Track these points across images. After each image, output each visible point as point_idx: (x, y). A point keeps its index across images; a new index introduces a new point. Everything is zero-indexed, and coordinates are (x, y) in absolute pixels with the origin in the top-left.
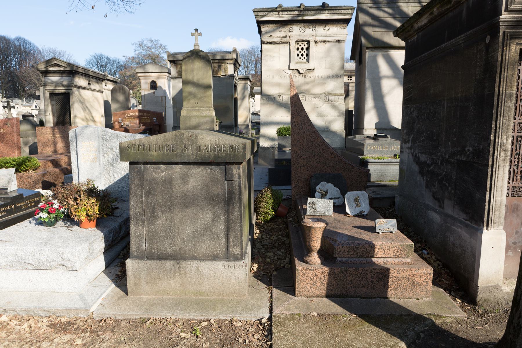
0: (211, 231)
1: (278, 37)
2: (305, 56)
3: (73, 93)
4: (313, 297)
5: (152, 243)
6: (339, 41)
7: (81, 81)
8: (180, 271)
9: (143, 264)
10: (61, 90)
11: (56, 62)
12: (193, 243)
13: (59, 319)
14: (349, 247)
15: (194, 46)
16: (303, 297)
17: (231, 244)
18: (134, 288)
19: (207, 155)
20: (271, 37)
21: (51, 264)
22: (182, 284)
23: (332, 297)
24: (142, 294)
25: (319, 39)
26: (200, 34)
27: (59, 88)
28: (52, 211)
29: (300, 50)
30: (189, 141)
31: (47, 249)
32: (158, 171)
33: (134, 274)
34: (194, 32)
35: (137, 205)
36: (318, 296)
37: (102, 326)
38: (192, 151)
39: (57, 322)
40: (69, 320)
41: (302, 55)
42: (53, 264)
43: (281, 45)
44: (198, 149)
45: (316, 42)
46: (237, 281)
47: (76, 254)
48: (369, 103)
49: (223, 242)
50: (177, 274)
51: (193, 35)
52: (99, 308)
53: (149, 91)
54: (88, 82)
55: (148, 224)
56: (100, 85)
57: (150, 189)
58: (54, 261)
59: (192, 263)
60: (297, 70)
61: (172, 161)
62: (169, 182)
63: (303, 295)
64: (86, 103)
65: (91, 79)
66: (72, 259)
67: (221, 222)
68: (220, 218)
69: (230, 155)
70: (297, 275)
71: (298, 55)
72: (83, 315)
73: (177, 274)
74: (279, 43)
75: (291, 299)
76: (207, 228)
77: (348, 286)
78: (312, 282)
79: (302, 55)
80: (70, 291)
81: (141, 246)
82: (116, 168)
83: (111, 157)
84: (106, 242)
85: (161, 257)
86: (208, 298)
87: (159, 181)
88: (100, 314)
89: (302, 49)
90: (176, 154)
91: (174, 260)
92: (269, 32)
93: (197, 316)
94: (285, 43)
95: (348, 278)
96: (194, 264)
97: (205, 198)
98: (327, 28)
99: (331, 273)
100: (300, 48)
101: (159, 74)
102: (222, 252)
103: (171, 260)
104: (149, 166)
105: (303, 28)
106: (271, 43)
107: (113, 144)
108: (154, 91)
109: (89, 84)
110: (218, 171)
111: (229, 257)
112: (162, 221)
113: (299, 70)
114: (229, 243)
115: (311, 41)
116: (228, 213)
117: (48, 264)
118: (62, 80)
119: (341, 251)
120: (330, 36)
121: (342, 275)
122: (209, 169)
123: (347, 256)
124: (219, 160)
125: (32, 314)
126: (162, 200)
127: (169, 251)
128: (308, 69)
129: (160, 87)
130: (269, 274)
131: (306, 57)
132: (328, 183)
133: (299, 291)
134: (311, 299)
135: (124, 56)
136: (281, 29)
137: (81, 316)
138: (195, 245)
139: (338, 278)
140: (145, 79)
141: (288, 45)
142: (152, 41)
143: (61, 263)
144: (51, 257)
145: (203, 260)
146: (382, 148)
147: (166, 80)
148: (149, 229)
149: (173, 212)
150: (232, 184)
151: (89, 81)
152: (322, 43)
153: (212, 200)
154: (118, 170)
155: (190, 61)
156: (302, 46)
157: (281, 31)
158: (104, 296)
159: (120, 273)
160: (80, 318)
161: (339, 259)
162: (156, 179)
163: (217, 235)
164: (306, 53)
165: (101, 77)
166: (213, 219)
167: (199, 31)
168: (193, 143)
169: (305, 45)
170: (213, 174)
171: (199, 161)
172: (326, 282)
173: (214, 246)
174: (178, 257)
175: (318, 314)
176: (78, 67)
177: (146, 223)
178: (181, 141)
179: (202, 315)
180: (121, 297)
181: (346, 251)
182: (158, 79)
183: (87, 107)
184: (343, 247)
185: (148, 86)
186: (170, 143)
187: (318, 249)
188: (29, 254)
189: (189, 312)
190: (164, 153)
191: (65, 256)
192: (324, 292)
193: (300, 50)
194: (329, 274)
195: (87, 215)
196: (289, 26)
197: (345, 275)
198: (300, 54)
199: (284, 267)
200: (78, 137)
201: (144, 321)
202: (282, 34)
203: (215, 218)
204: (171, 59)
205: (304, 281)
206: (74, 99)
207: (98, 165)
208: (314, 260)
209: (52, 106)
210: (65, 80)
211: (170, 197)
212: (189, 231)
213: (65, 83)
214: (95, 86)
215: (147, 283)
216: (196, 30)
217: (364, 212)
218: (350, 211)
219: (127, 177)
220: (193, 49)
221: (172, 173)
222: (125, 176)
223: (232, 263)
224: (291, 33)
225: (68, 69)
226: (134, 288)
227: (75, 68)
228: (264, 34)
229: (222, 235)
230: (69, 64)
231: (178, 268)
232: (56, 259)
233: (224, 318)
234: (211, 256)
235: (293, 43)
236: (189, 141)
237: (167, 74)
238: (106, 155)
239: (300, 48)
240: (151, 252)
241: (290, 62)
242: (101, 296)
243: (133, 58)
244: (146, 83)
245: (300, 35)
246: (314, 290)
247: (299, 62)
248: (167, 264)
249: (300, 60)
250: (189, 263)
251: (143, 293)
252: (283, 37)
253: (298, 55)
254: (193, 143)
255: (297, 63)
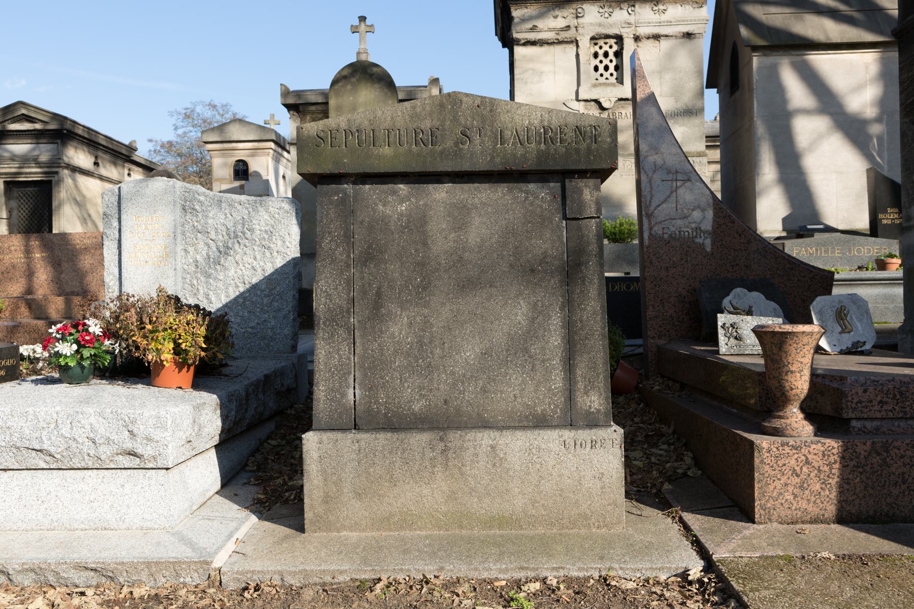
0: (526, 350)
1: (550, 30)
2: (612, 69)
3: (60, 181)
4: (803, 522)
5: (371, 388)
6: (688, 36)
7: (80, 157)
8: (447, 460)
9: (348, 443)
10: (33, 173)
11: (24, 111)
12: (481, 383)
13: (125, 590)
14: (881, 391)
15: (358, 53)
16: (775, 524)
17: (581, 385)
18: (320, 509)
19: (520, 151)
20: (534, 29)
21: (102, 449)
22: (452, 496)
23: (856, 522)
24: (344, 528)
25: (643, 31)
26: (371, 29)
27: (28, 170)
28: (87, 342)
29: (601, 57)
30: (474, 119)
31: (91, 410)
32: (390, 198)
33: (323, 472)
34: (356, 22)
35: (336, 289)
36: (815, 521)
37: (252, 600)
38: (482, 142)
39: (122, 596)
40: (153, 592)
41: (606, 68)
42: (105, 451)
43: (558, 49)
44: (496, 138)
45: (637, 39)
46: (599, 485)
47: (169, 422)
48: (768, 172)
49: (558, 381)
50: (438, 468)
51: (354, 30)
52: (233, 559)
53: (231, 183)
54: (93, 160)
55: (363, 336)
56: (120, 169)
57: (370, 247)
58: (108, 441)
59: (480, 435)
60: (597, 102)
61: (516, 71)
62: (417, 224)
63: (774, 517)
64: (89, 206)
65: (100, 154)
66: (157, 435)
67: (552, 328)
68: (550, 317)
69: (577, 151)
70: (757, 461)
71: (596, 69)
72: (193, 578)
73: (438, 468)
74: (553, 43)
75: (748, 528)
76: (521, 347)
77: (896, 491)
78: (798, 480)
79: (606, 68)
80: (149, 524)
81: (344, 395)
82: (216, 279)
83: (204, 253)
84: (224, 418)
85: (395, 423)
86: (522, 532)
87: (392, 223)
88: (242, 573)
89: (606, 55)
90: (442, 153)
91: (431, 428)
92: (531, 18)
93: (507, 570)
94: (567, 42)
95: (893, 469)
96: (485, 439)
97: (512, 266)
98: (661, 7)
99: (847, 455)
100: (601, 52)
101: (256, 144)
102: (556, 406)
103: (423, 430)
104: (367, 186)
105: (606, 9)
106: (533, 43)
107: (210, 221)
108: (243, 182)
109: (96, 164)
110: (542, 195)
111: (572, 418)
112: (399, 328)
113: (602, 100)
114: (576, 383)
115: (625, 36)
116: (570, 305)
117: (92, 453)
118: (36, 153)
119: (860, 402)
120: (669, 23)
121: (876, 460)
122: (521, 191)
123: (878, 415)
124: (552, 166)
125: (52, 579)
126: (401, 274)
127: (417, 407)
128: (621, 99)
129: (257, 174)
130: (654, 491)
131: (615, 73)
132: (750, 290)
133: (763, 508)
134: (798, 526)
135: (150, 141)
136: (557, 12)
137: (188, 580)
138: (484, 390)
139: (868, 469)
140: (223, 156)
141: (571, 49)
142: (215, 106)
143: (129, 445)
144: (102, 430)
145: (508, 428)
146: (826, 251)
147: (270, 160)
148: (365, 349)
149: (426, 305)
150: (579, 228)
151: (96, 157)
152: (651, 41)
153: (530, 272)
154: (220, 285)
155: (349, 87)
156: (606, 48)
157: (556, 17)
158: (240, 535)
159: (262, 497)
160: (185, 585)
161: (854, 423)
162: (385, 219)
163: (543, 361)
164: (614, 63)
165: (124, 152)
166: (532, 320)
167: (368, 22)
168: (483, 122)
169: (611, 47)
170: (532, 204)
171: (500, 168)
172: (834, 481)
173: (536, 391)
174: (443, 422)
175: (837, 556)
176: (74, 122)
177: (357, 334)
178: (455, 119)
179: (522, 568)
180: (286, 537)
181: (875, 403)
182: (253, 155)
183: (89, 216)
184: (865, 391)
185: (229, 172)
186: (427, 124)
187: (802, 397)
188: (43, 424)
189: (483, 562)
190: (410, 151)
191: (140, 429)
192: (831, 509)
193: (601, 57)
194: (843, 458)
195: (177, 346)
196: (574, 6)
197: (884, 460)
198: (601, 67)
199: (685, 475)
200: (123, 206)
201: (363, 587)
202: (560, 23)
203: (538, 313)
204: (291, 101)
205: (776, 478)
206: (62, 194)
207: (171, 273)
208: (795, 425)
209: (10, 212)
210: (45, 152)
211: (422, 264)
212: (470, 352)
213: (44, 158)
214: (110, 171)
215: (358, 496)
216: (363, 19)
217: (864, 343)
218: (829, 343)
219: (241, 300)
220: (354, 60)
221: (426, 205)
222: (236, 299)
223: (585, 435)
224: (580, 20)
225: (53, 126)
226: (320, 509)
227: (68, 126)
228: (519, 23)
229: (556, 362)
230: (55, 116)
231: (443, 451)
232: (114, 437)
233: (581, 575)
234: (527, 417)
235: (585, 42)
236: (474, 119)
237: (272, 145)
238: (191, 249)
239: (601, 52)
240: (368, 411)
241: (579, 84)
242: (230, 536)
243: (170, 143)
244: (225, 165)
245: (600, 25)
246: (804, 504)
247: (600, 84)
248: (412, 441)
249: (602, 80)
250: (471, 435)
251: (347, 523)
252: (562, 30)
253: (596, 69)
254: (483, 122)
255: (595, 86)
